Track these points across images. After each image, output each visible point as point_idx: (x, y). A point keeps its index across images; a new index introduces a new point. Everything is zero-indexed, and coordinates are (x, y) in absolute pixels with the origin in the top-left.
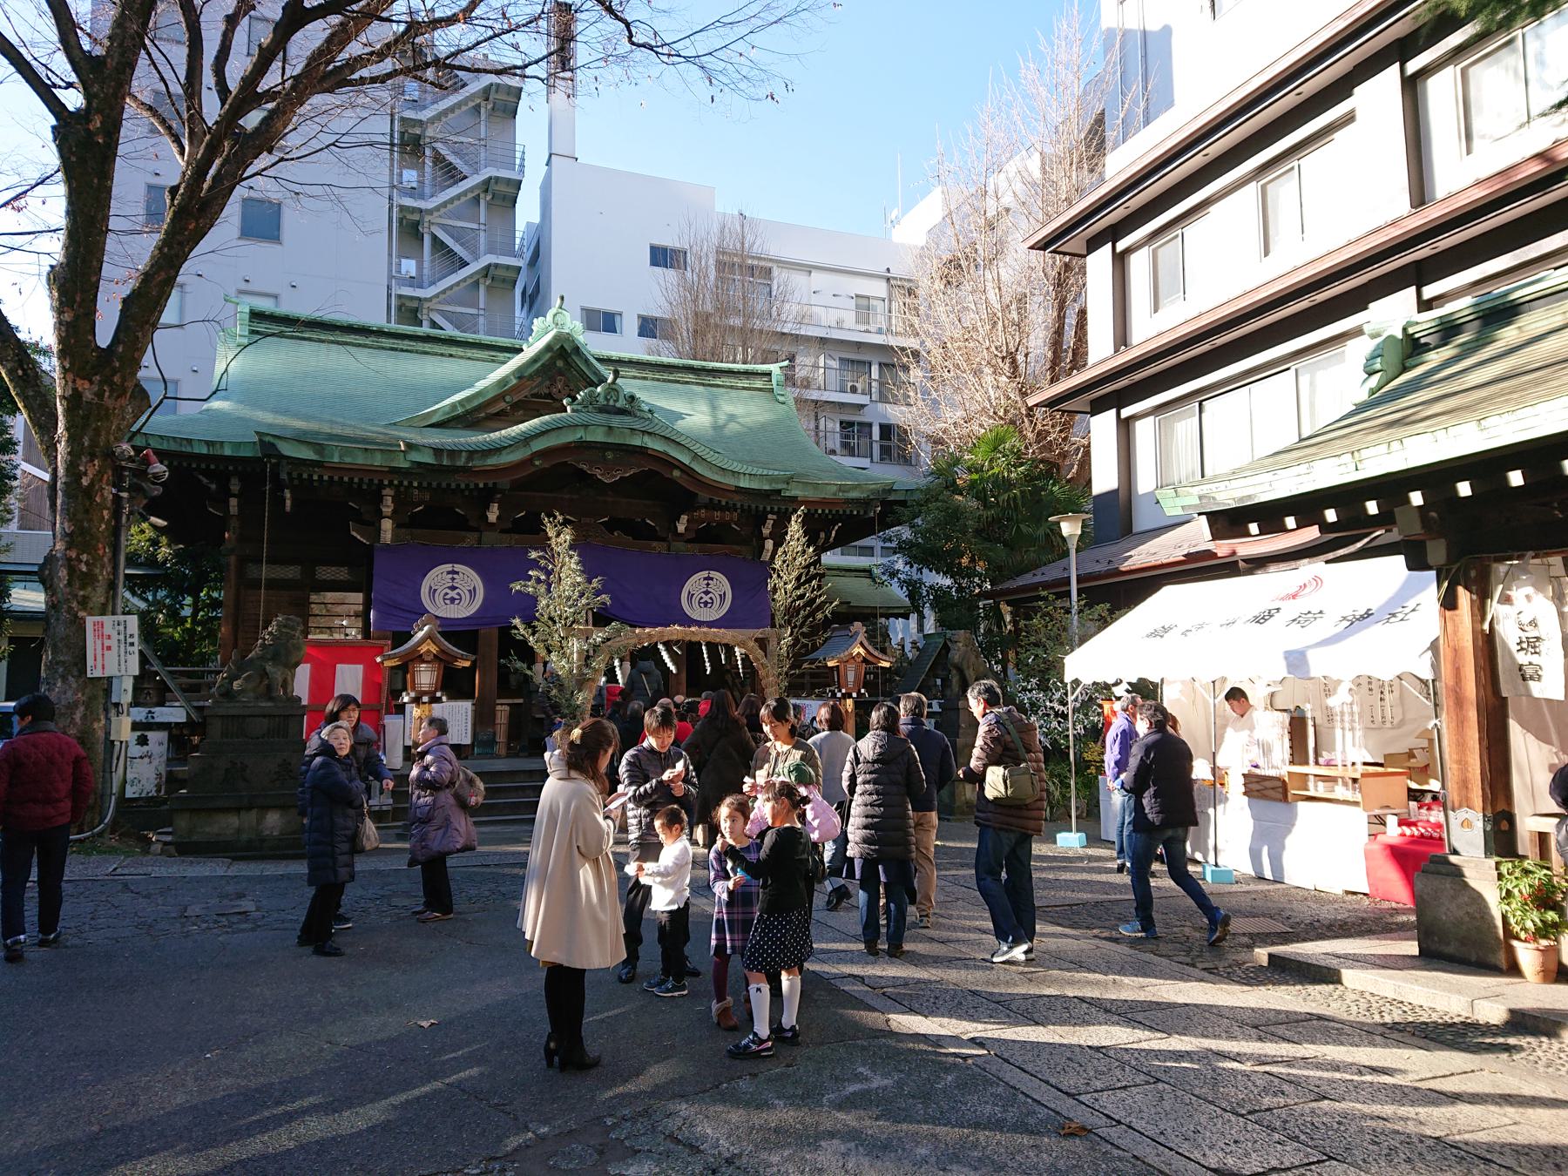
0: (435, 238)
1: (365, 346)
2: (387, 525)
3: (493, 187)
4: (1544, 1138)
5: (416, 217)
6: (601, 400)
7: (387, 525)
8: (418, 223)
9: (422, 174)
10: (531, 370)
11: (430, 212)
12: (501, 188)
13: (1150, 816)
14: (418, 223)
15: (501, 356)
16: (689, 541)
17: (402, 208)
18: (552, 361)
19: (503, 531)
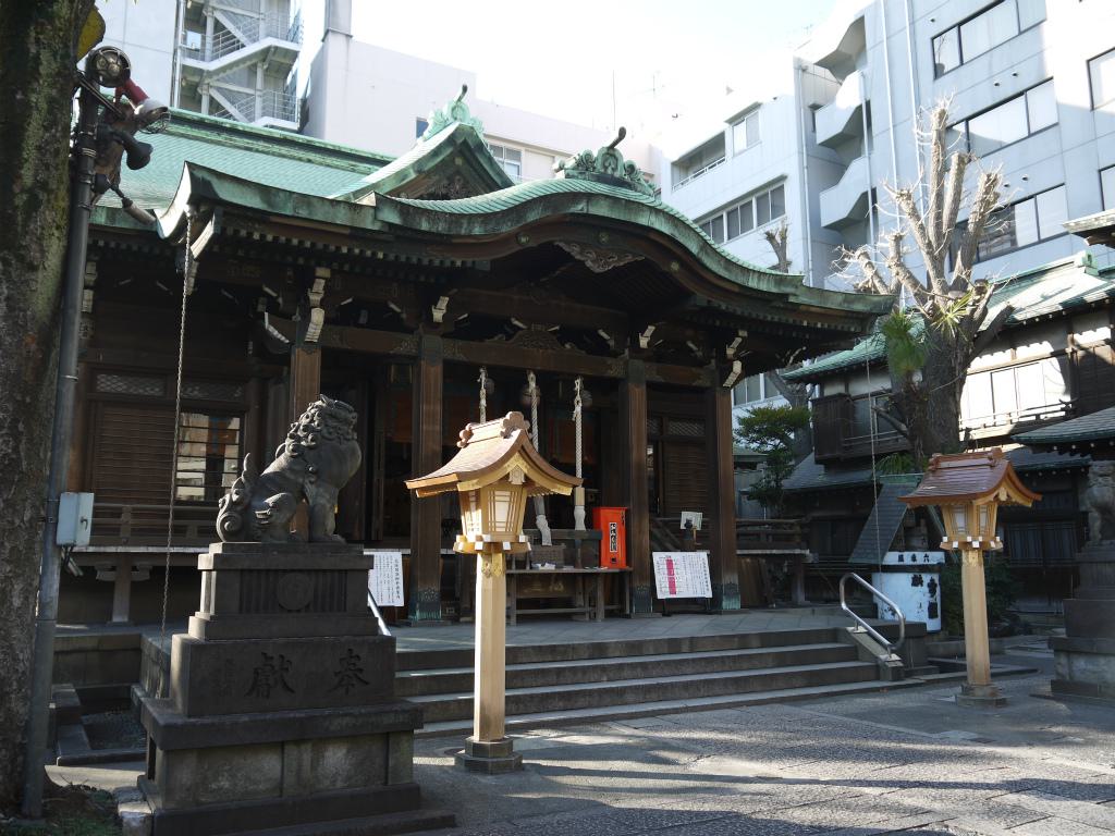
0: (212, 100)
1: (218, 143)
2: (318, 316)
3: (270, 57)
4: (577, 767)
5: (196, 79)
6: (598, 165)
7: (318, 316)
8: (197, 85)
9: (204, 38)
10: (431, 164)
11: (210, 74)
12: (278, 59)
13: (75, 573)
14: (197, 85)
15: (363, 166)
16: (647, 359)
17: (185, 68)
18: (452, 157)
19: (444, 336)
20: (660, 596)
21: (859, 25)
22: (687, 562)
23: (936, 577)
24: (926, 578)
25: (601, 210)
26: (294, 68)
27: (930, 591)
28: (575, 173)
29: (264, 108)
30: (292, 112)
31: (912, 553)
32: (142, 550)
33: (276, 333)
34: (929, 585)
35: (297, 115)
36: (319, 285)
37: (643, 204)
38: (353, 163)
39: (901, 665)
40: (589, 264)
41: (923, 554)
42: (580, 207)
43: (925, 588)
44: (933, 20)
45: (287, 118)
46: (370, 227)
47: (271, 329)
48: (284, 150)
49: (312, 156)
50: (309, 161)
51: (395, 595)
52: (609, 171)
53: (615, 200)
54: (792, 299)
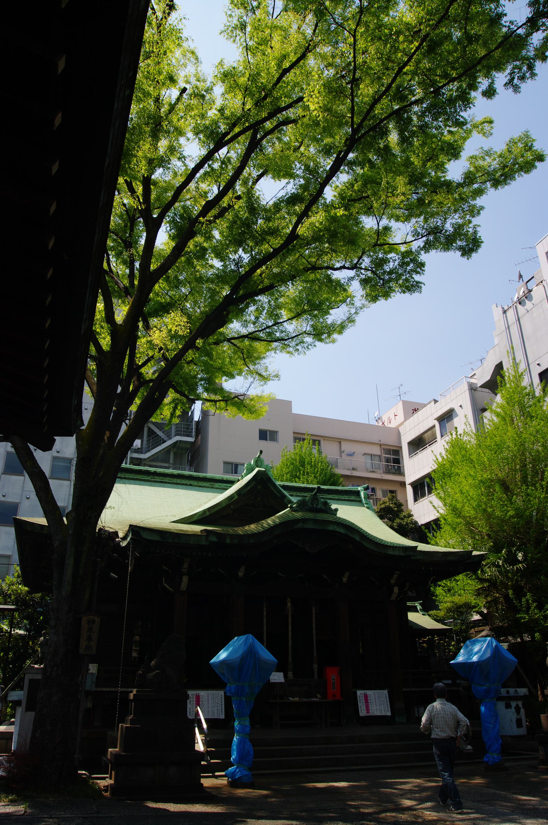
0: (149, 429)
2: (185, 579)
6: (309, 504)
7: (185, 579)
10: (245, 491)
20: (361, 714)
21: (499, 367)
22: (376, 696)
23: (520, 704)
24: (513, 704)
25: (310, 526)
26: (193, 408)
27: (516, 712)
28: (298, 509)
29: (176, 431)
30: (191, 432)
31: (506, 689)
32: (108, 689)
33: (168, 587)
34: (515, 708)
35: (194, 434)
36: (186, 565)
37: (330, 521)
38: (212, 483)
39: (472, 751)
40: (307, 549)
41: (514, 690)
42: (300, 525)
43: (513, 710)
44: (538, 364)
45: (188, 436)
46: (204, 544)
47: (166, 585)
48: (179, 481)
49: (192, 482)
50: (191, 485)
51: (221, 712)
52: (315, 506)
53: (316, 521)
54: (413, 558)
